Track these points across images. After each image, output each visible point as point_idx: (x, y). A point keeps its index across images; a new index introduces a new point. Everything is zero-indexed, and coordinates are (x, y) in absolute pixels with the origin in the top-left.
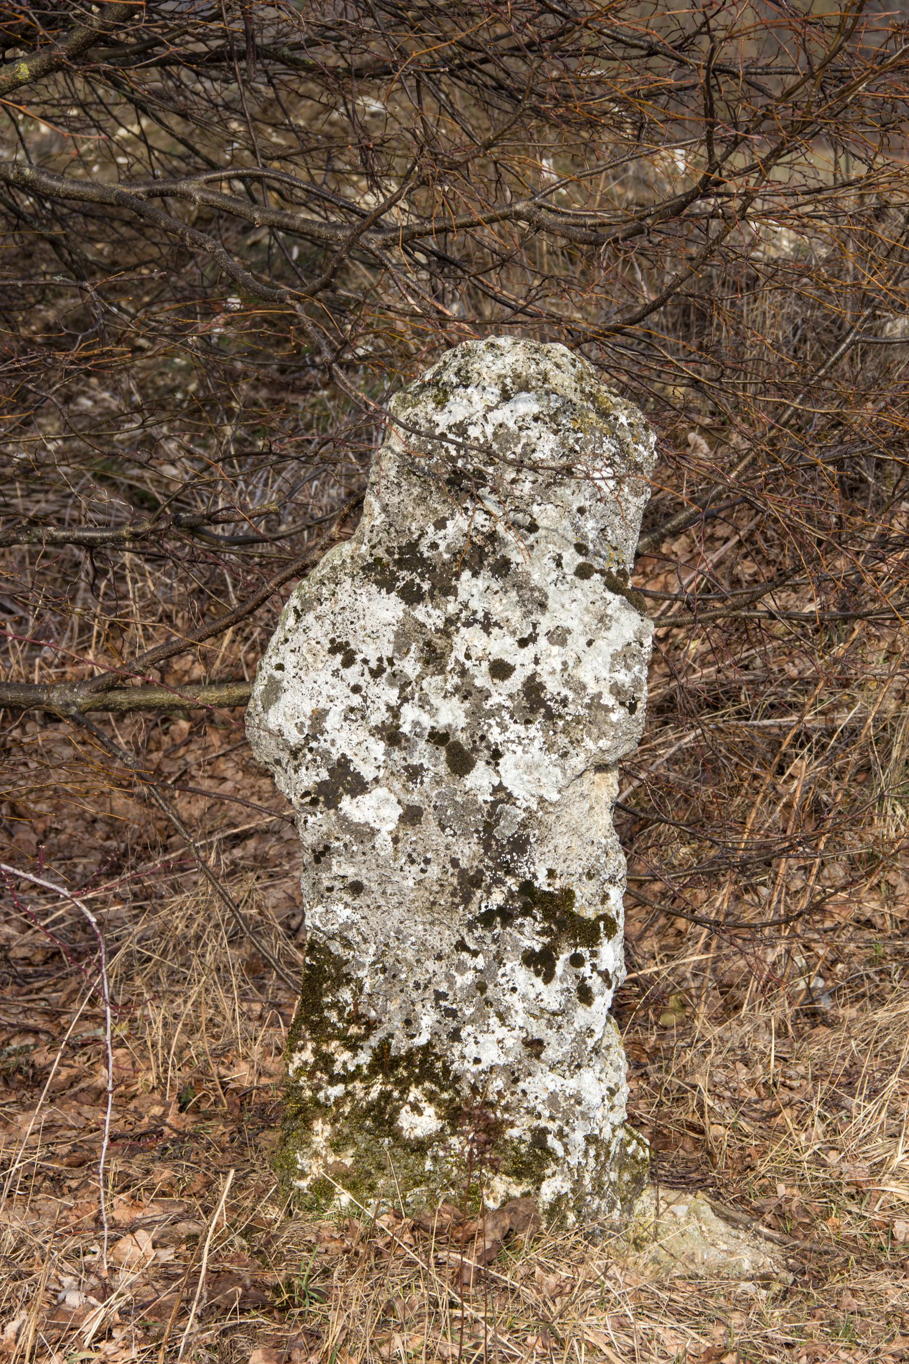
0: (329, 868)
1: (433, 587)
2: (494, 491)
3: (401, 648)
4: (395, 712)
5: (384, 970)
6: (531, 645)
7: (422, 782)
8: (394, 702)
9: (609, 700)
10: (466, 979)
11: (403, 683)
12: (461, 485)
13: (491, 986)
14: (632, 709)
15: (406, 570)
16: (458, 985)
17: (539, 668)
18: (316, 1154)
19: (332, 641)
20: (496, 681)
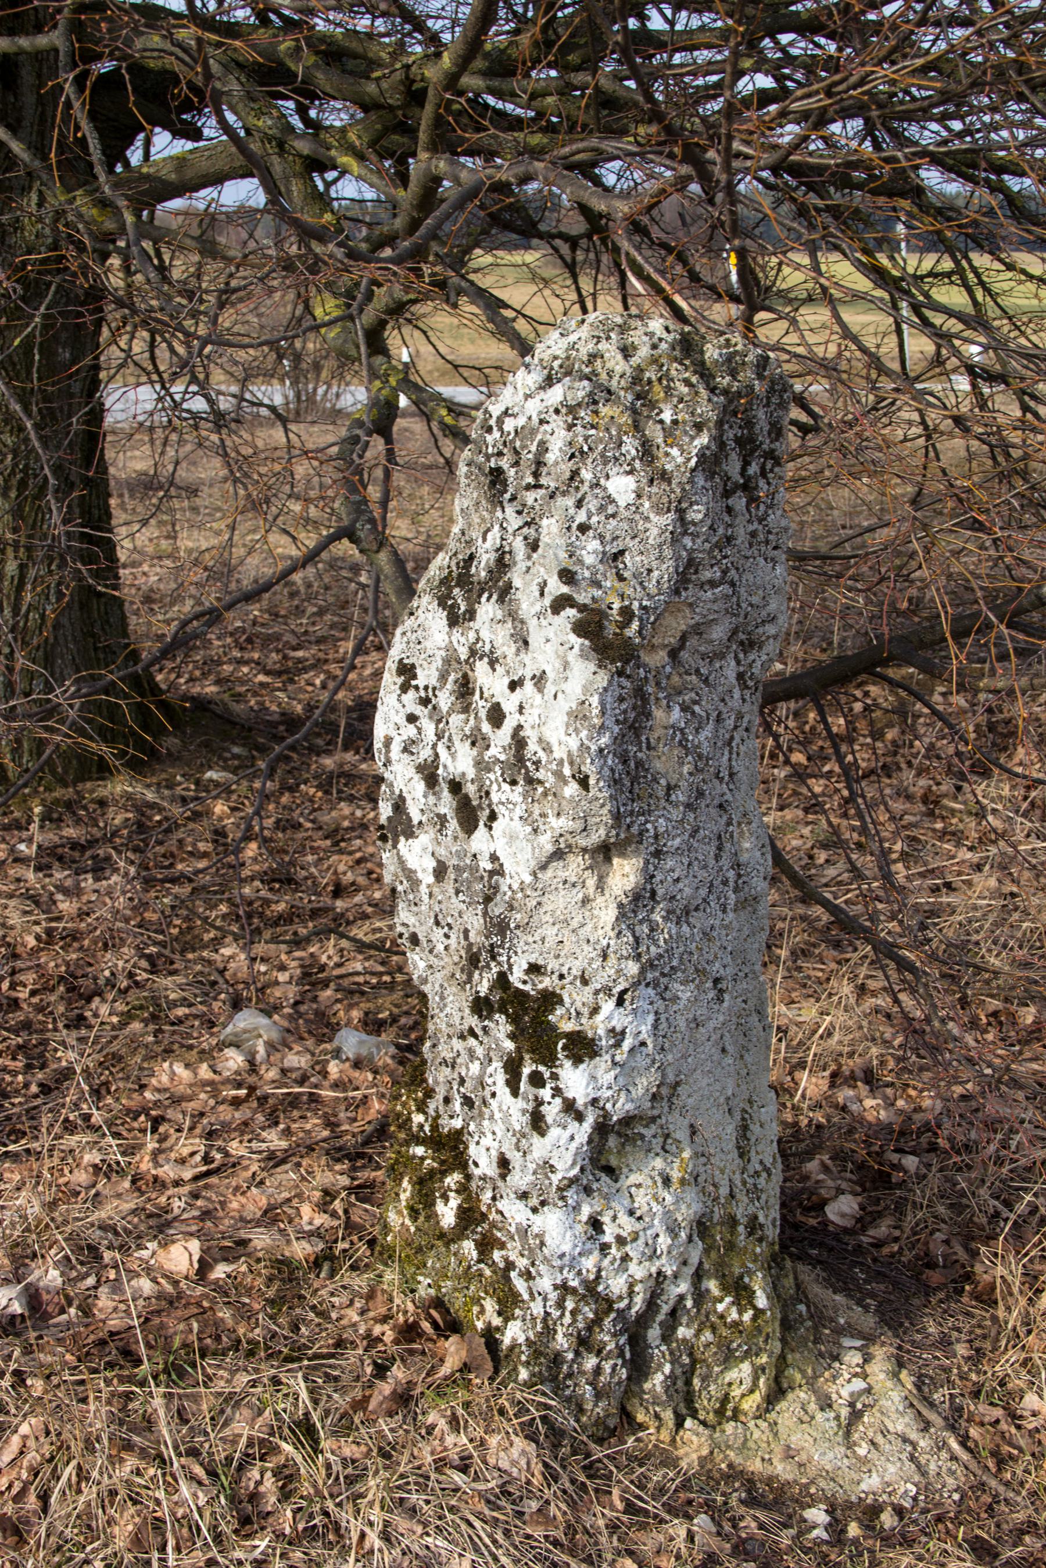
3: (443, 677)
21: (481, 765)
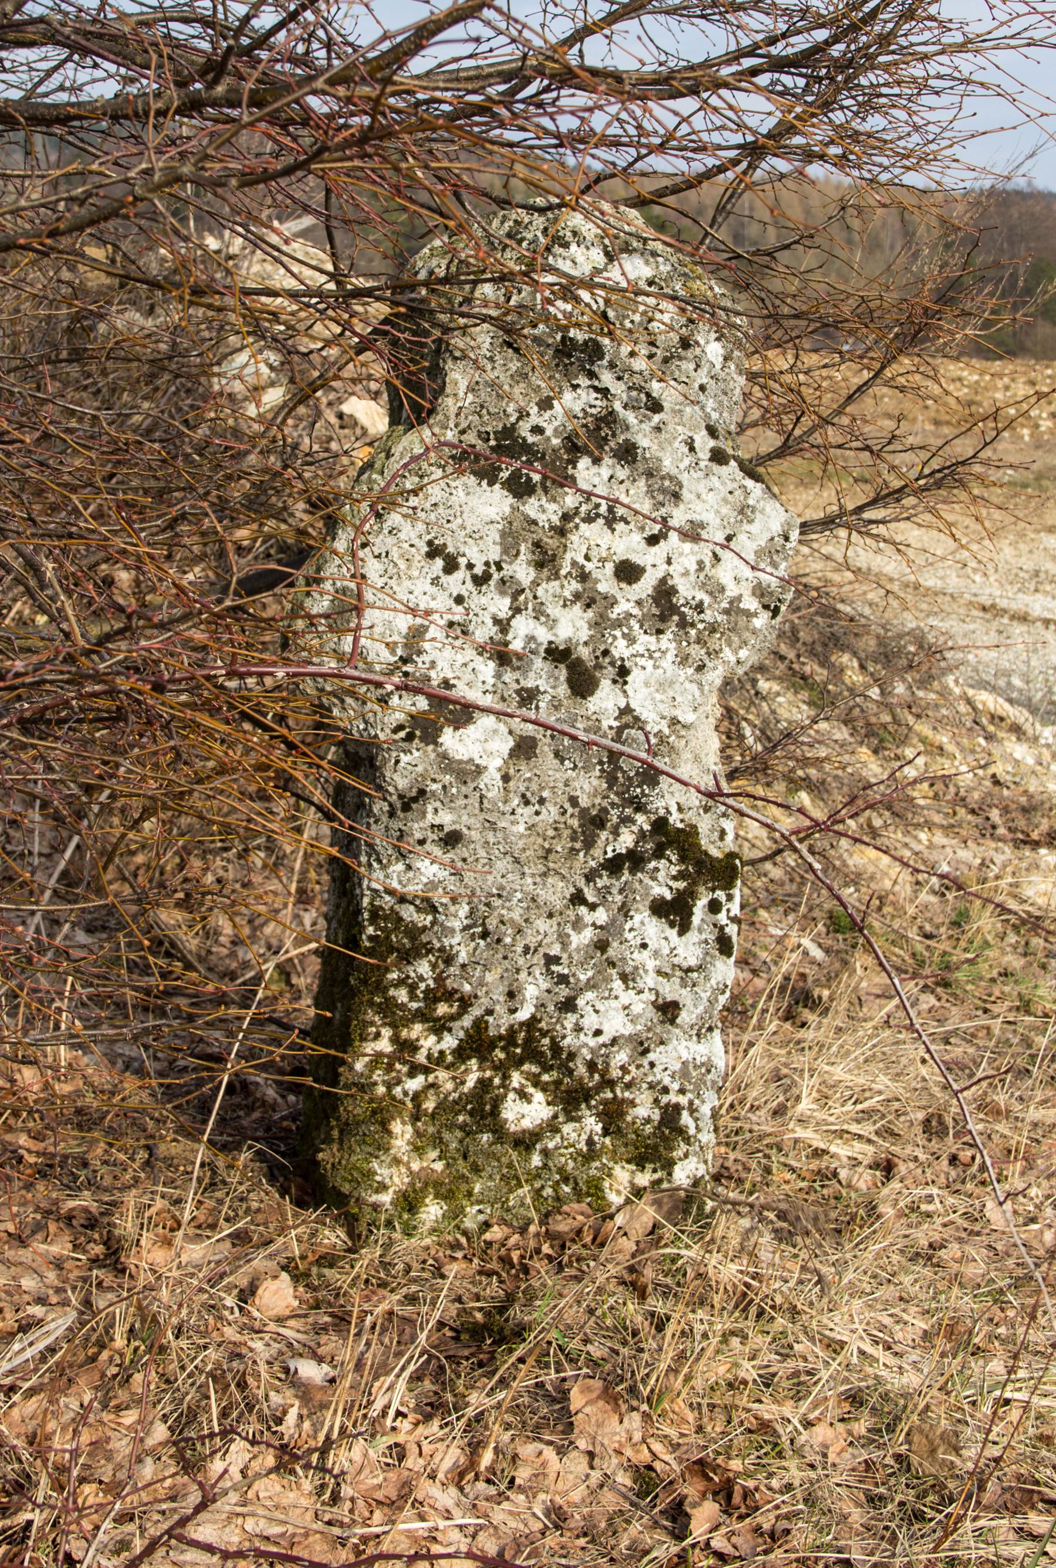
0: (424, 814)
1: (545, 477)
4: (503, 625)
5: (485, 935)
6: (662, 543)
7: (537, 708)
8: (504, 612)
9: (750, 603)
12: (575, 357)
13: (615, 944)
14: (776, 612)
15: (503, 457)
16: (574, 946)
18: (397, 1161)
19: (430, 543)
20: (623, 585)
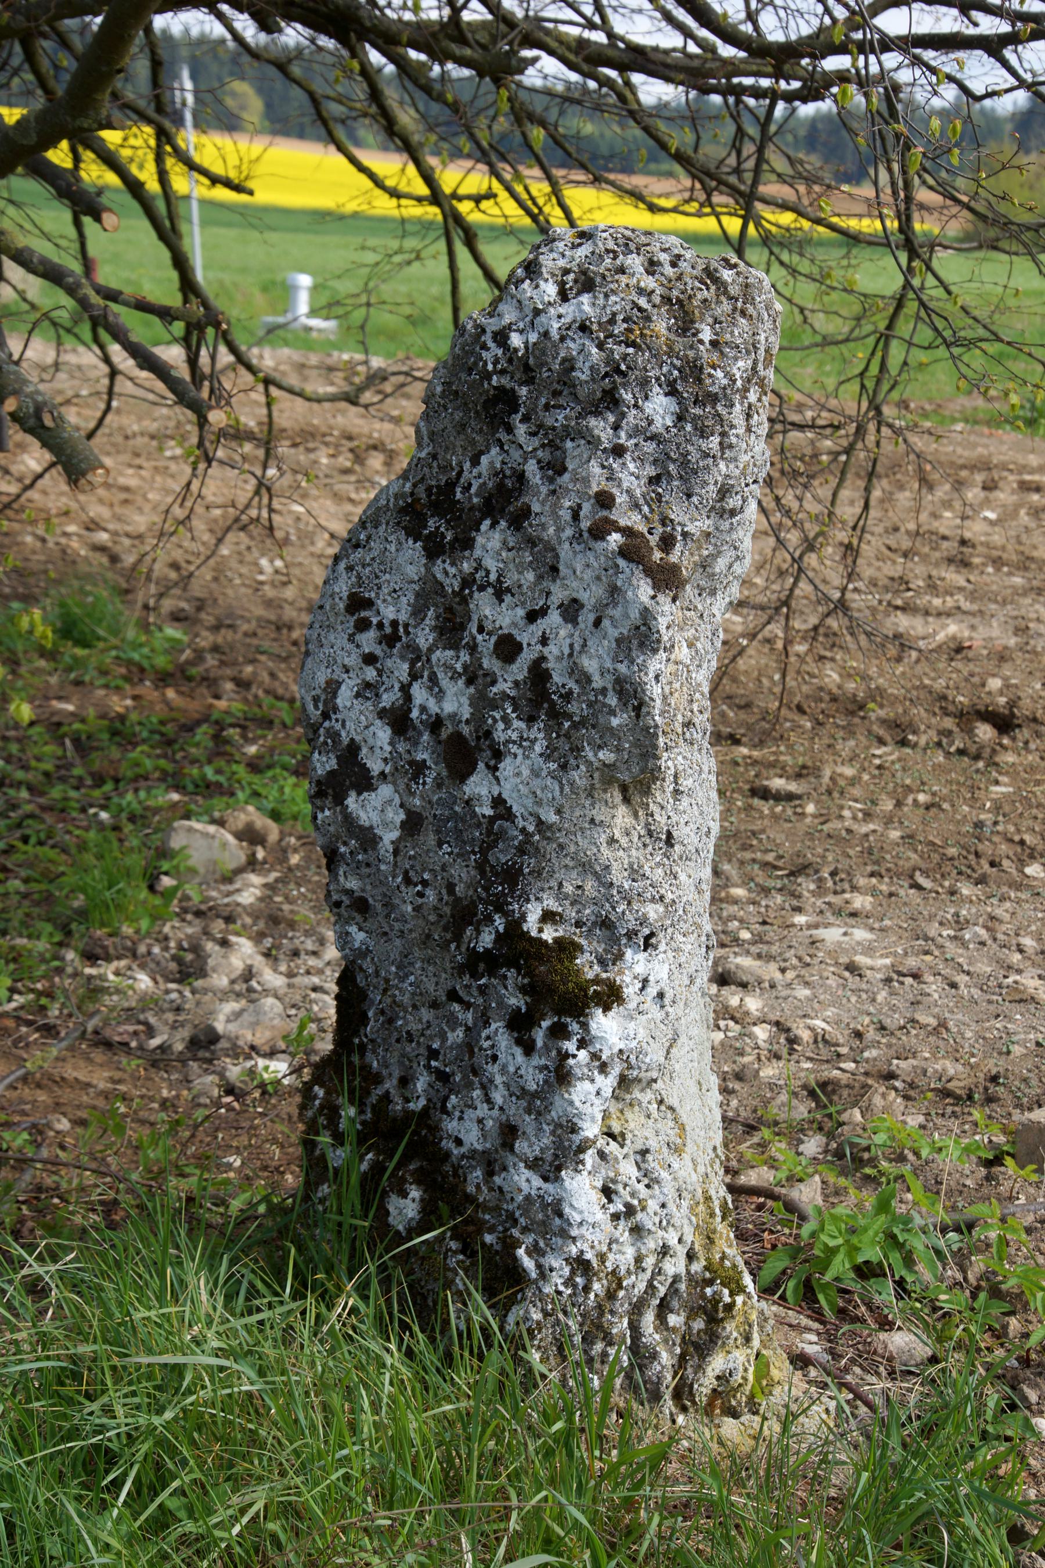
2: (526, 419)
3: (418, 612)
10: (457, 1036)
11: (416, 656)
17: (546, 651)
21: (483, 703)
